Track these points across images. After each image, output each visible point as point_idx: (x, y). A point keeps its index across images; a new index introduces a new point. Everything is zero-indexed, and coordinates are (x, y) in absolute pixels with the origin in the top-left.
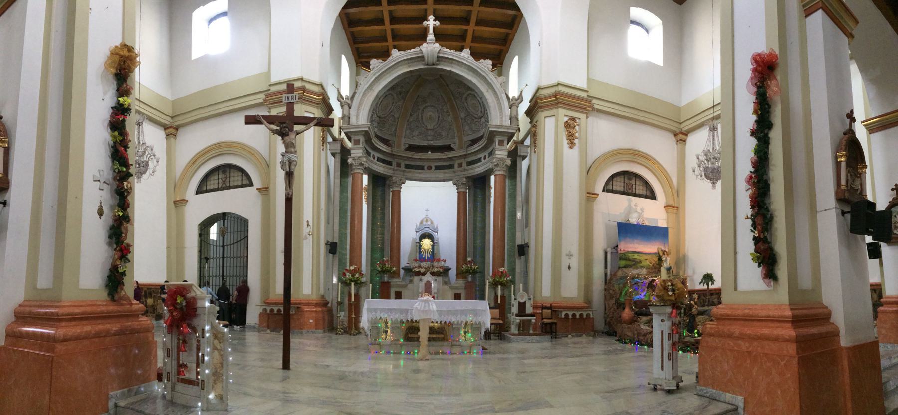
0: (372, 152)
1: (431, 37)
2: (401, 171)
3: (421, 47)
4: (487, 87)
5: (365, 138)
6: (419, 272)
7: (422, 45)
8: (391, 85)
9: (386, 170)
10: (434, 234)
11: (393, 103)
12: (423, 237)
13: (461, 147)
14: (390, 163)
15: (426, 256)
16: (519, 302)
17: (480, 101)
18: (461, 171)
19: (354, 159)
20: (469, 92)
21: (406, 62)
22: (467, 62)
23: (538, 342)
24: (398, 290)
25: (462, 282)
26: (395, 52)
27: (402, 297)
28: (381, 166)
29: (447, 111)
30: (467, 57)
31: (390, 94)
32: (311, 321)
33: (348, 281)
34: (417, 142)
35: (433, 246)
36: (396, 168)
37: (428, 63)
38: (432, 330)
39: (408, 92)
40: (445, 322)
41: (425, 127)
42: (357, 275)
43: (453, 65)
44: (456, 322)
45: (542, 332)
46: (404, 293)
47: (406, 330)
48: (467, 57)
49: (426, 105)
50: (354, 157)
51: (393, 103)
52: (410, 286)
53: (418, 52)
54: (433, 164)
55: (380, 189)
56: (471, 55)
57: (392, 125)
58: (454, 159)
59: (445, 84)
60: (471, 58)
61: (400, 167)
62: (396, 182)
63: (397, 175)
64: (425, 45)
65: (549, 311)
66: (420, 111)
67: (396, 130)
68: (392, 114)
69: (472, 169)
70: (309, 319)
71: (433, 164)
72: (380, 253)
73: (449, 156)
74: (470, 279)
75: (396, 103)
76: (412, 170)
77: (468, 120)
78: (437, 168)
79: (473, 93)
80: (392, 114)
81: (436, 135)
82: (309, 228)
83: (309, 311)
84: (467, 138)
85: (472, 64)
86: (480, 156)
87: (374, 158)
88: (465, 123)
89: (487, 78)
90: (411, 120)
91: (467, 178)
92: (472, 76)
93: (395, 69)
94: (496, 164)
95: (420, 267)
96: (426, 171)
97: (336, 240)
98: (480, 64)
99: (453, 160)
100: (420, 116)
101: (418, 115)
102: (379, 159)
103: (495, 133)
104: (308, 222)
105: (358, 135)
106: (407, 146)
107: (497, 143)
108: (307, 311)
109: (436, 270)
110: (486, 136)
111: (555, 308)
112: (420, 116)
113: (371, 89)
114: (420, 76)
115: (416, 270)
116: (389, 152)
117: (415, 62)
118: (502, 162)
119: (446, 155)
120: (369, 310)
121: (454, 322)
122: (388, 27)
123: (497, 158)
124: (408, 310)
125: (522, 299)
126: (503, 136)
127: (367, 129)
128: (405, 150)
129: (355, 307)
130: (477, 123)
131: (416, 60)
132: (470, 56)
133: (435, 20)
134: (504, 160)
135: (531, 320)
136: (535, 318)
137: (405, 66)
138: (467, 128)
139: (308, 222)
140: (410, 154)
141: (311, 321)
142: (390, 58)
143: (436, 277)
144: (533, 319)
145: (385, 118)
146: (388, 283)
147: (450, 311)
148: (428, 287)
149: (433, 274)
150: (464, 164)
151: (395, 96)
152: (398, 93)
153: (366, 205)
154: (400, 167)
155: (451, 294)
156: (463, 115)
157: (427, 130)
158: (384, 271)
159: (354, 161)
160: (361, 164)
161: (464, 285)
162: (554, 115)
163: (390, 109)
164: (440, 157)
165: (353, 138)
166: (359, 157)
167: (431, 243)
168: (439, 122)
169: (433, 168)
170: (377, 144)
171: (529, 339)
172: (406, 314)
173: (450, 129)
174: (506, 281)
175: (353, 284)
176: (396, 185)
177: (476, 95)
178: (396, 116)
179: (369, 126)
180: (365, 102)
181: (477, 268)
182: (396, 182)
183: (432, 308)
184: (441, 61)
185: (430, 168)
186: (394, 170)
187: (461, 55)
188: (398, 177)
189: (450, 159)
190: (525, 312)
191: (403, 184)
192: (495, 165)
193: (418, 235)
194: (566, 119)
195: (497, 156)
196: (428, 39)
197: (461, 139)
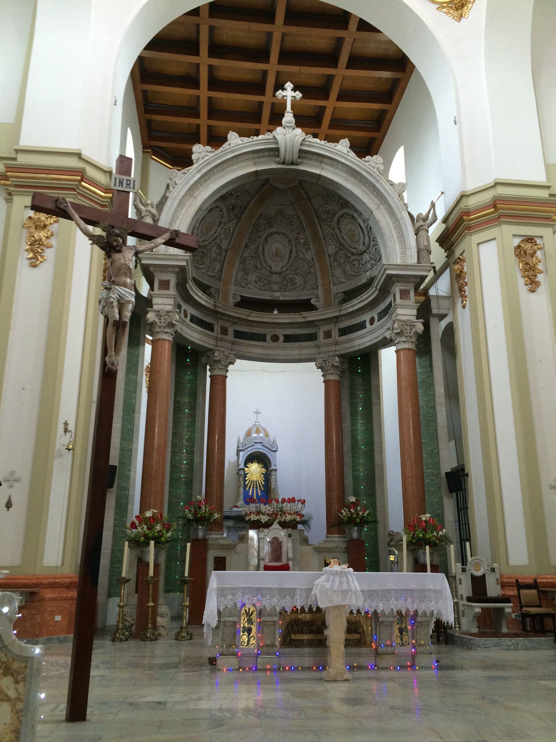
0: (185, 306)
1: (289, 117)
2: (228, 341)
3: (274, 132)
4: (378, 202)
5: (178, 279)
6: (258, 521)
7: (275, 129)
8: (223, 192)
9: (204, 338)
11: (221, 223)
12: (250, 459)
13: (328, 304)
14: (209, 327)
16: (472, 576)
17: (362, 225)
18: (330, 345)
19: (158, 313)
20: (344, 210)
21: (251, 156)
22: (346, 159)
23: (527, 649)
24: (220, 554)
25: (337, 539)
26: (233, 137)
27: (227, 566)
28: (195, 331)
29: (306, 243)
30: (346, 152)
31: (217, 207)
32: (58, 618)
33: (142, 539)
34: (253, 293)
36: (220, 336)
37: (285, 159)
39: (245, 208)
40: (358, 611)
41: (268, 268)
42: (158, 527)
43: (323, 166)
44: (387, 612)
45: (524, 629)
47: (287, 627)
48: (346, 152)
49: (273, 230)
50: (159, 311)
51: (221, 223)
52: (240, 547)
53: (270, 141)
54: (281, 333)
56: (350, 147)
57: (215, 260)
58: (316, 324)
59: (306, 198)
60: (352, 154)
61: (227, 335)
62: (220, 360)
63: (221, 349)
64: (279, 129)
65: (534, 591)
66: (262, 241)
67: (221, 270)
68: (217, 241)
69: (351, 340)
70: (53, 614)
71: (281, 333)
72: (184, 487)
73: (309, 319)
75: (225, 224)
76: (247, 342)
77: (340, 257)
78: (288, 339)
79: (351, 212)
80: (217, 241)
81: (285, 282)
82: (68, 435)
83: (55, 599)
84: (337, 289)
85: (354, 163)
86: (362, 320)
87: (186, 316)
88: (335, 264)
89: (378, 185)
90: (246, 255)
91: (341, 356)
92: (353, 183)
93: (233, 165)
94: (399, 331)
95: (259, 513)
96: (269, 343)
98: (366, 164)
99: (317, 326)
100: (261, 249)
101: (258, 247)
102: (193, 319)
103: (394, 279)
104: (66, 424)
105: (168, 272)
106: (239, 299)
107: (398, 296)
108: (50, 599)
110: (378, 283)
111: (545, 587)
112: (261, 249)
113: (191, 196)
114: (267, 181)
115: (253, 517)
116: (211, 307)
117: (263, 156)
118: (408, 328)
119: (304, 317)
120: (222, 592)
121: (383, 611)
123: (400, 320)
124: (295, 589)
125: (478, 570)
126: (409, 282)
127: (184, 263)
128: (235, 306)
129: (153, 586)
130: (355, 262)
131: (266, 154)
132: (349, 150)
133: (294, 90)
135: (502, 609)
136: (511, 604)
137: (250, 163)
138: (338, 272)
139: (66, 424)
140: (242, 313)
141: (58, 618)
142: (226, 145)
143: (290, 530)
144: (508, 608)
145: (205, 247)
146: (205, 541)
147: (375, 591)
149: (284, 525)
150: (335, 333)
151: (225, 210)
152: (231, 207)
153: (91, 420)
154: (227, 335)
156: (331, 250)
157: (271, 273)
158: (199, 520)
159: (160, 319)
160: (171, 325)
161: (343, 546)
162: (495, 239)
163: (215, 233)
164: (293, 321)
165: (159, 277)
166: (168, 312)
168: (291, 260)
169: (282, 338)
170: (193, 290)
171: (509, 643)
172: (293, 597)
173: (309, 273)
174: (437, 538)
175: (152, 543)
176: (220, 367)
177: (356, 215)
178: (224, 246)
179: (188, 258)
180: (181, 216)
181: (368, 514)
182: (220, 360)
183: (355, 587)
184: (305, 158)
185: (275, 338)
186: (217, 340)
187: (336, 148)
188: (223, 352)
189: (311, 324)
190: (486, 594)
191: (231, 366)
192: (397, 334)
193: (243, 456)
194: (516, 241)
195: (399, 317)
196: (284, 120)
197: (327, 291)
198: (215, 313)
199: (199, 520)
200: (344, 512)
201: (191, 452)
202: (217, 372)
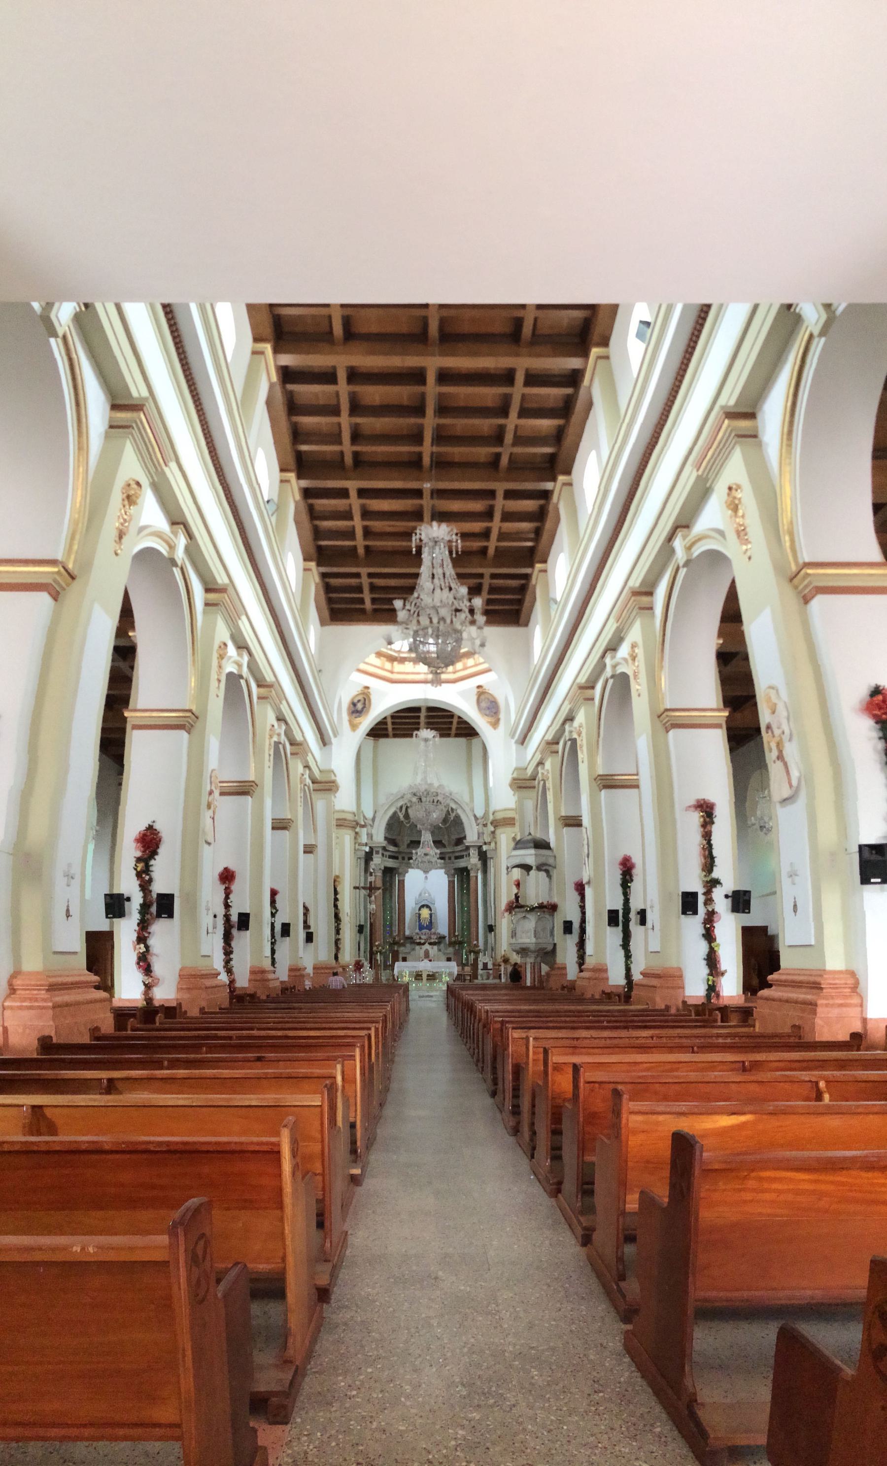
10: (431, 906)
15: (425, 923)
35: (431, 915)
38: (428, 975)
42: (380, 948)
46: (408, 958)
55: (388, 875)
74: (457, 948)
97: (362, 923)
109: (432, 941)
115: (418, 941)
120: (398, 967)
122: (355, 503)
134: (476, 865)
146: (397, 951)
148: (427, 955)
149: (430, 944)
150: (453, 858)
155: (444, 958)
158: (395, 943)
167: (430, 912)
198: (399, 852)
199: (395, 943)
200: (453, 939)
201: (391, 913)
202: (401, 879)
